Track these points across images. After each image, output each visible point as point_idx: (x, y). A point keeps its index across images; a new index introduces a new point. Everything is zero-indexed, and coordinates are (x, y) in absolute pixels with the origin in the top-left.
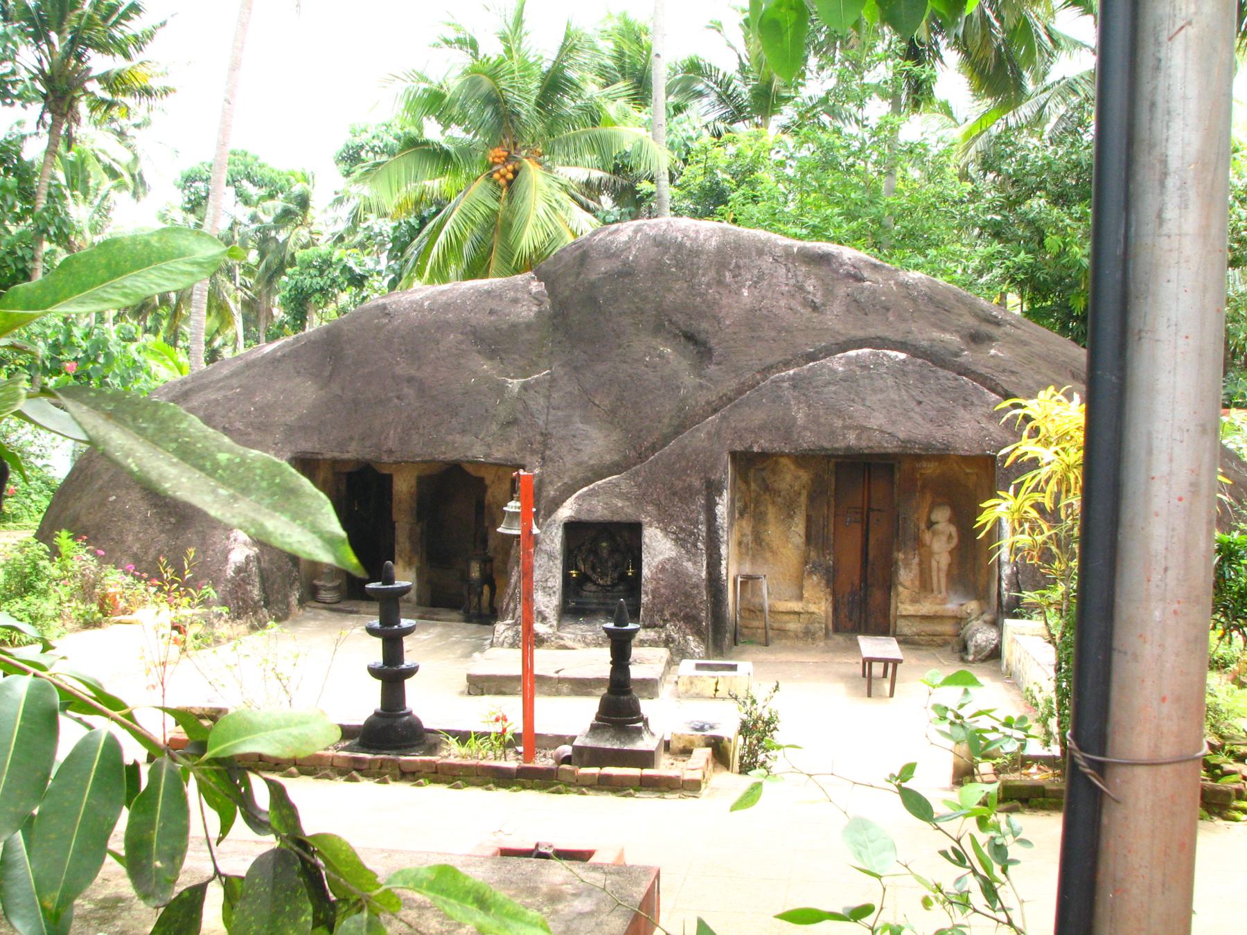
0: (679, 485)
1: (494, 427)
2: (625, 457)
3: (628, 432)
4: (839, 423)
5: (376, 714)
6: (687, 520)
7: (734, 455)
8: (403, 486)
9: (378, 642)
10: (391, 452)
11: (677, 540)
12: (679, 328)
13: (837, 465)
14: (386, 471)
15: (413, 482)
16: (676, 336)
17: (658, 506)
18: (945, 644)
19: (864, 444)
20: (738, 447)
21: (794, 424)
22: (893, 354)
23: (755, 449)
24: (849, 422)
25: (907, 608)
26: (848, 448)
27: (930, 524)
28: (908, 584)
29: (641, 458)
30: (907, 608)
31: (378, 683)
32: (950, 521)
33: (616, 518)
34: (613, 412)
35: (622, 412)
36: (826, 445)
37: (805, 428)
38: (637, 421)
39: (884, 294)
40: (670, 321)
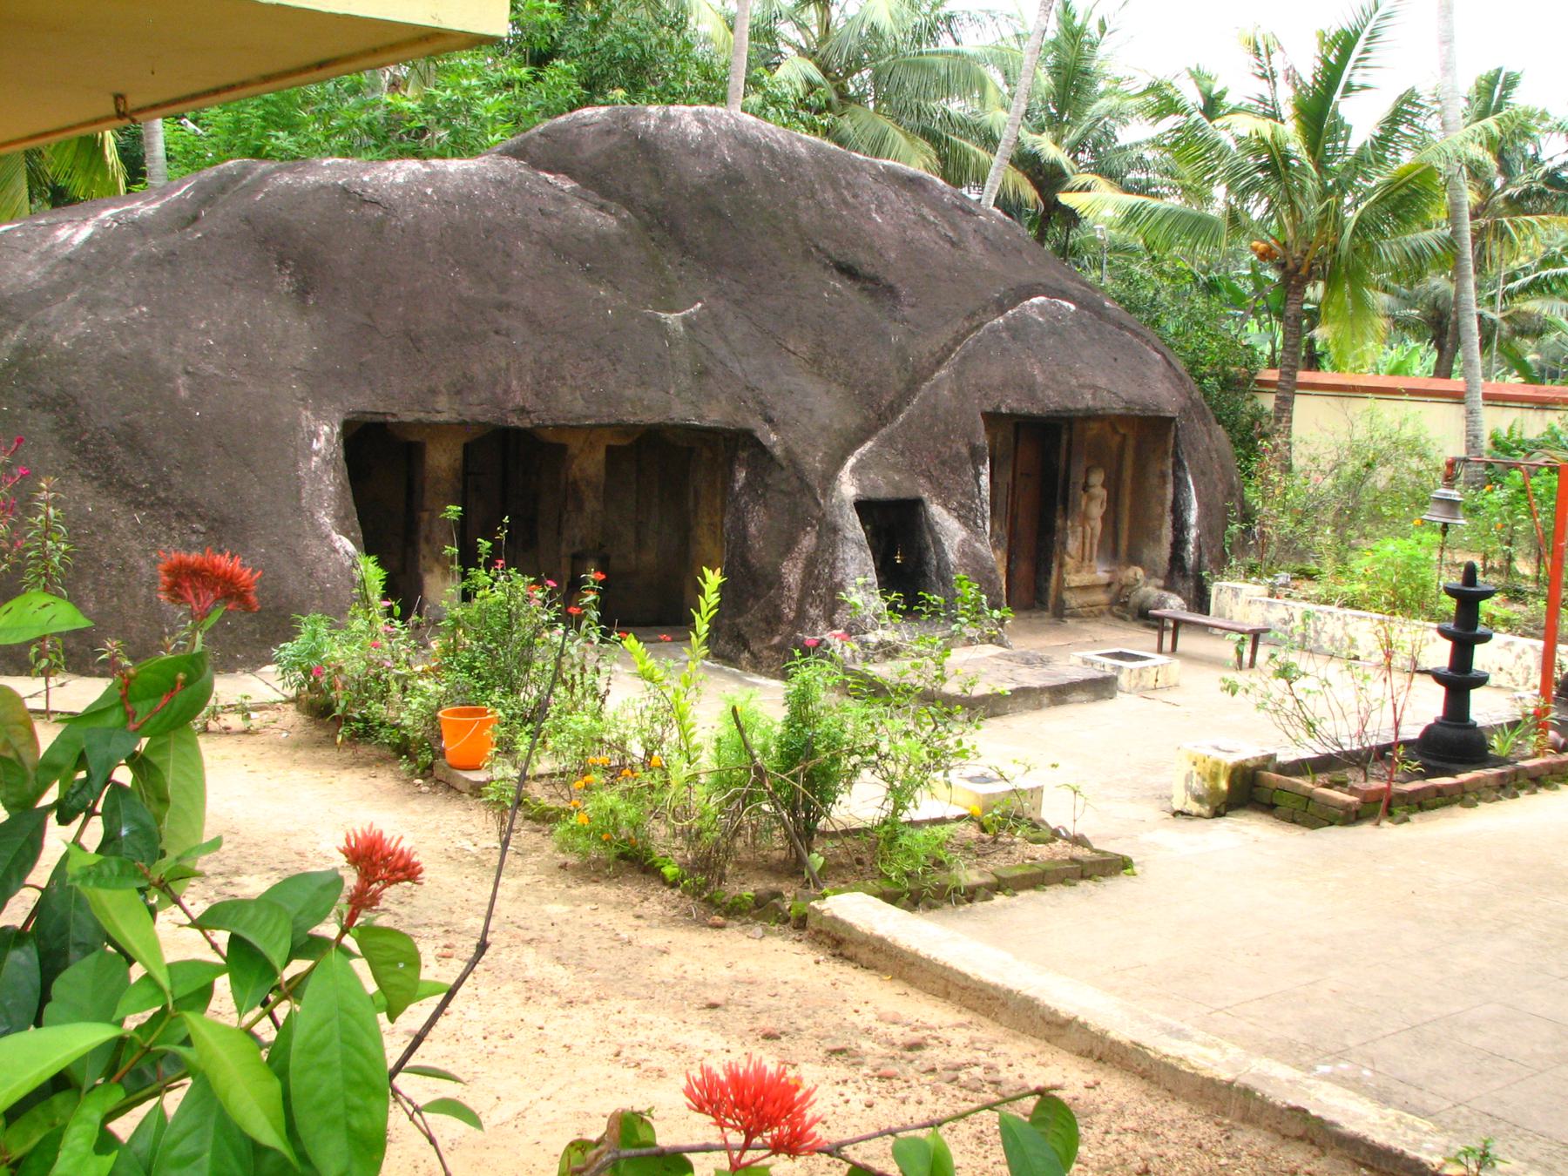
0: (946, 452)
1: (685, 381)
2: (866, 418)
3: (853, 387)
4: (1074, 382)
5: (1437, 722)
6: (964, 493)
7: (985, 415)
8: (442, 459)
9: (1448, 645)
10: (523, 411)
11: (959, 517)
12: (829, 257)
13: (1017, 425)
14: (414, 438)
15: (459, 453)
16: (826, 267)
17: (930, 478)
18: (1101, 613)
19: (1099, 405)
20: (989, 409)
21: (1034, 383)
22: (1066, 304)
23: (1004, 410)
24: (1082, 380)
25: (1074, 579)
26: (1088, 409)
27: (1086, 487)
28: (1073, 553)
29: (883, 418)
30: (1074, 579)
31: (1441, 691)
32: (1103, 486)
33: (902, 496)
34: (816, 361)
35: (829, 362)
36: (1071, 406)
37: (1048, 387)
38: (857, 374)
39: (373, 187)
40: (817, 247)
